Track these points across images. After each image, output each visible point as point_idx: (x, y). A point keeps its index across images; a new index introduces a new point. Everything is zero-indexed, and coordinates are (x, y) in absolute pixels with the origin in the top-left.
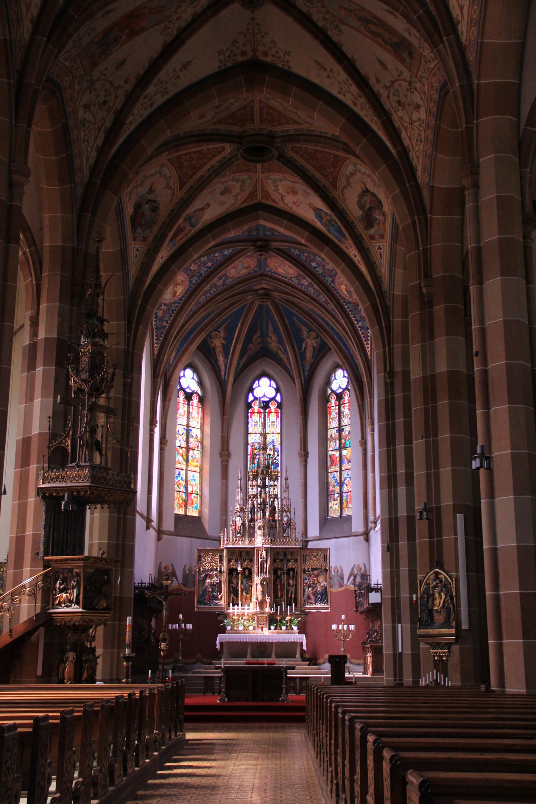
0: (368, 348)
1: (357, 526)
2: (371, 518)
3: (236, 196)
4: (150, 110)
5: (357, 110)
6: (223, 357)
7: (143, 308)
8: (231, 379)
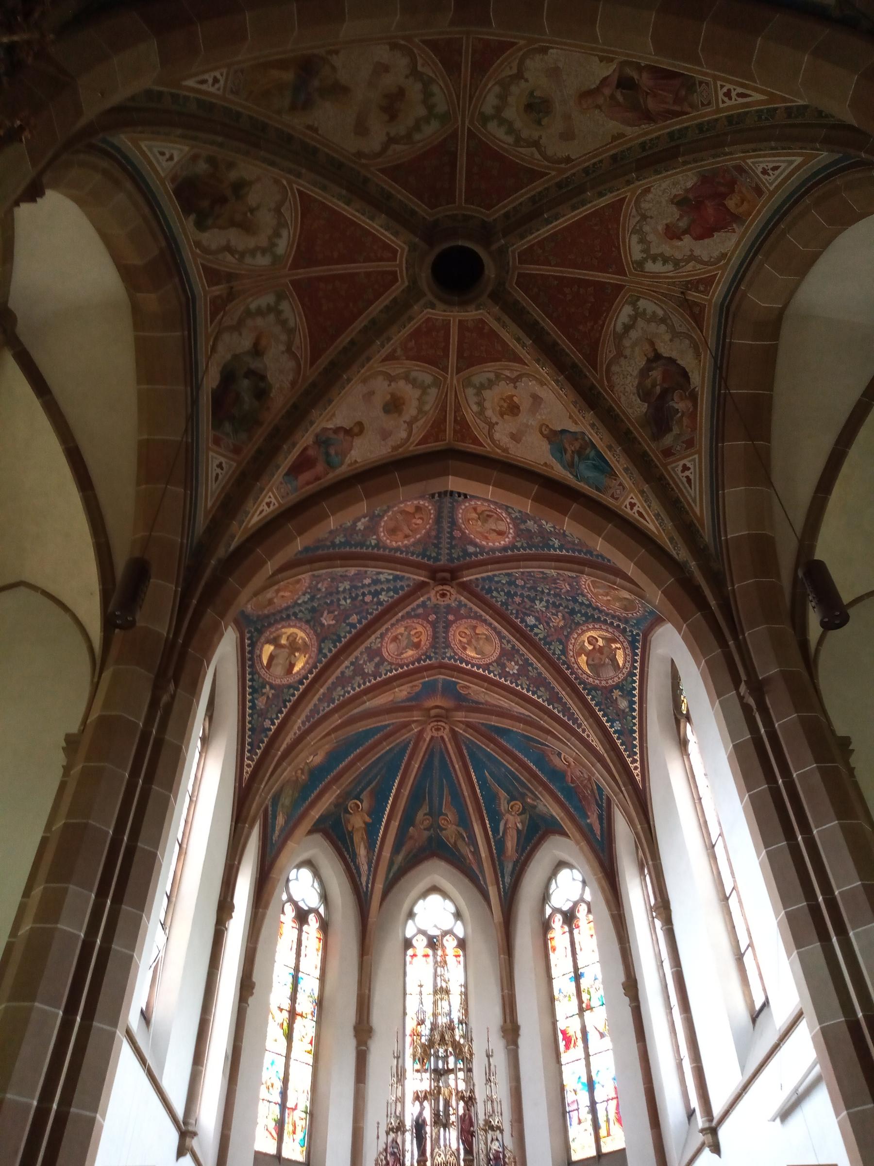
0: (636, 768)
3: (410, 424)
6: (365, 847)
8: (379, 887)
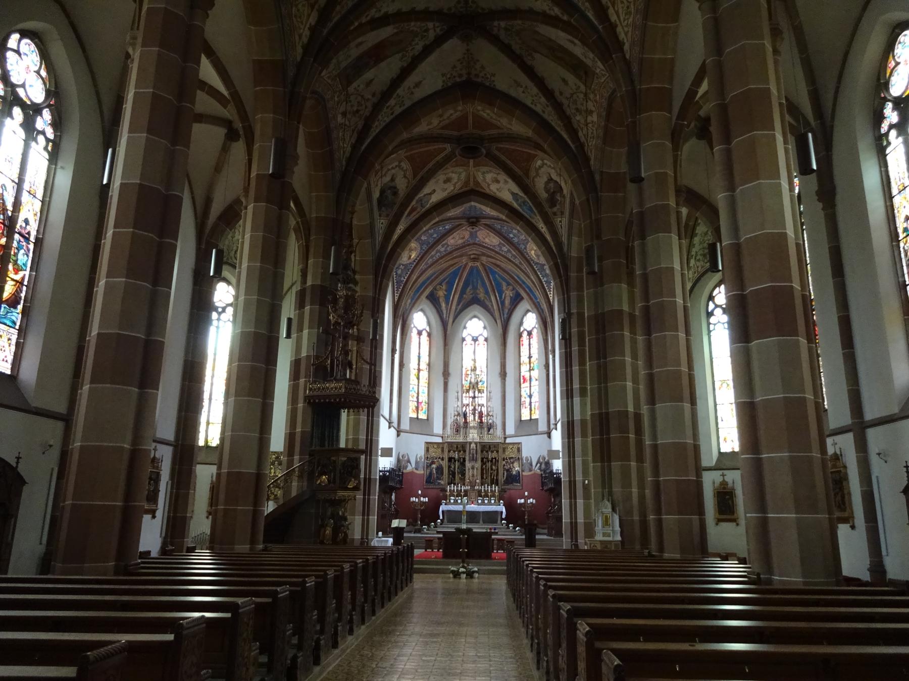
1: (542, 427)
2: (552, 421)
3: (455, 185)
4: (392, 117)
5: (545, 116)
7: (386, 266)
